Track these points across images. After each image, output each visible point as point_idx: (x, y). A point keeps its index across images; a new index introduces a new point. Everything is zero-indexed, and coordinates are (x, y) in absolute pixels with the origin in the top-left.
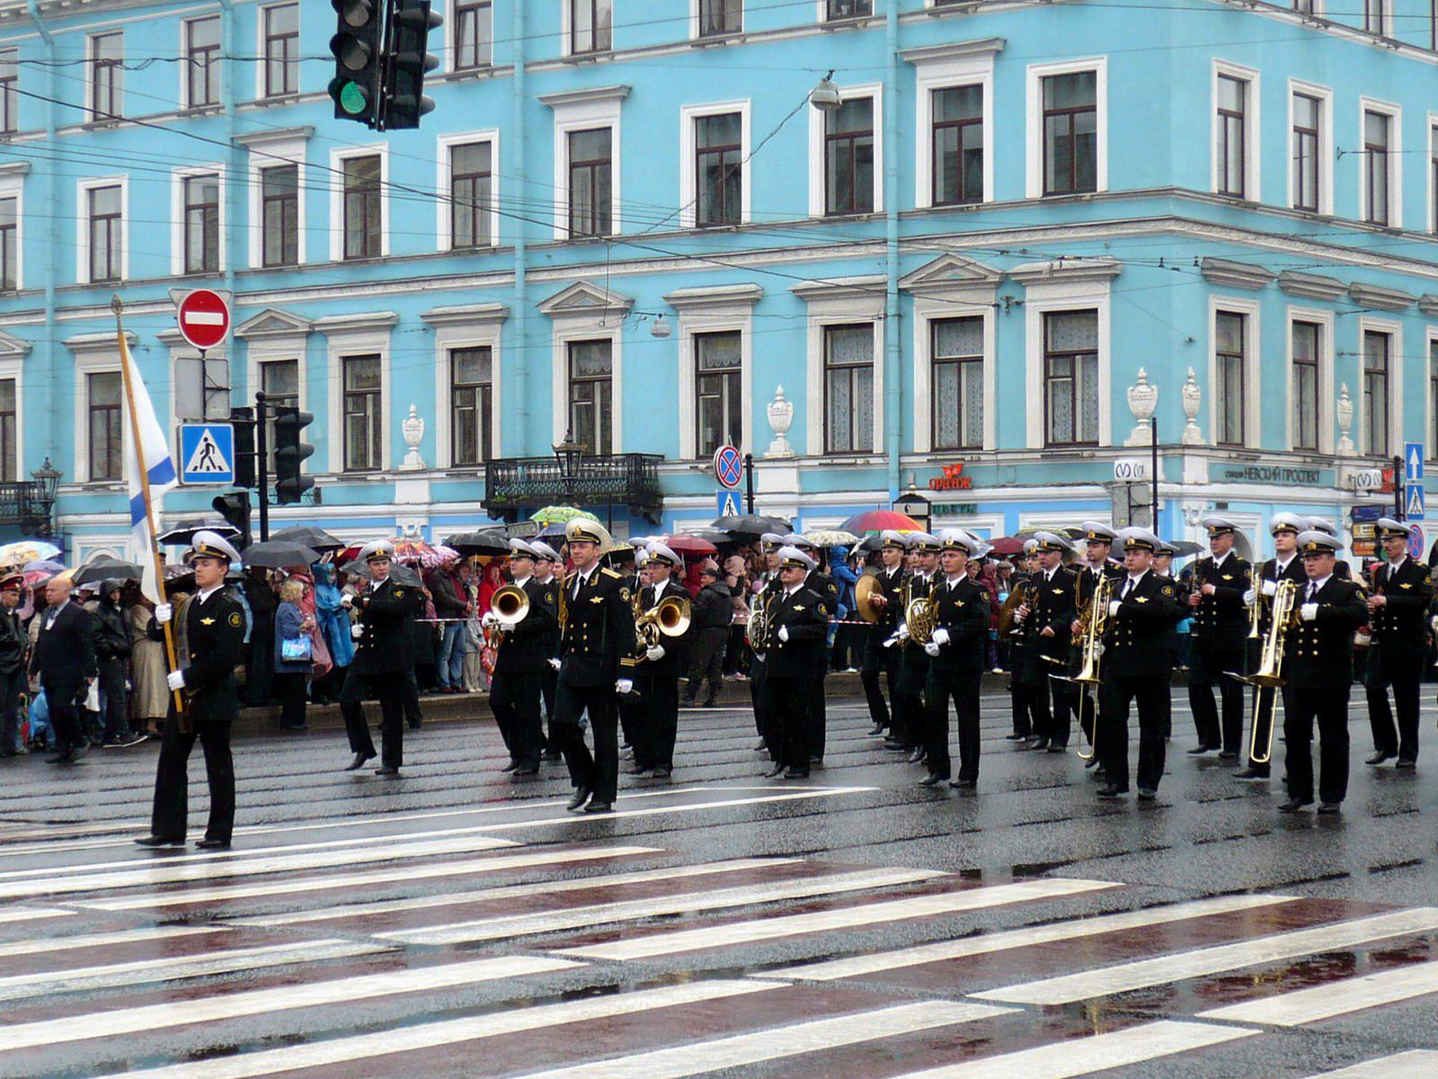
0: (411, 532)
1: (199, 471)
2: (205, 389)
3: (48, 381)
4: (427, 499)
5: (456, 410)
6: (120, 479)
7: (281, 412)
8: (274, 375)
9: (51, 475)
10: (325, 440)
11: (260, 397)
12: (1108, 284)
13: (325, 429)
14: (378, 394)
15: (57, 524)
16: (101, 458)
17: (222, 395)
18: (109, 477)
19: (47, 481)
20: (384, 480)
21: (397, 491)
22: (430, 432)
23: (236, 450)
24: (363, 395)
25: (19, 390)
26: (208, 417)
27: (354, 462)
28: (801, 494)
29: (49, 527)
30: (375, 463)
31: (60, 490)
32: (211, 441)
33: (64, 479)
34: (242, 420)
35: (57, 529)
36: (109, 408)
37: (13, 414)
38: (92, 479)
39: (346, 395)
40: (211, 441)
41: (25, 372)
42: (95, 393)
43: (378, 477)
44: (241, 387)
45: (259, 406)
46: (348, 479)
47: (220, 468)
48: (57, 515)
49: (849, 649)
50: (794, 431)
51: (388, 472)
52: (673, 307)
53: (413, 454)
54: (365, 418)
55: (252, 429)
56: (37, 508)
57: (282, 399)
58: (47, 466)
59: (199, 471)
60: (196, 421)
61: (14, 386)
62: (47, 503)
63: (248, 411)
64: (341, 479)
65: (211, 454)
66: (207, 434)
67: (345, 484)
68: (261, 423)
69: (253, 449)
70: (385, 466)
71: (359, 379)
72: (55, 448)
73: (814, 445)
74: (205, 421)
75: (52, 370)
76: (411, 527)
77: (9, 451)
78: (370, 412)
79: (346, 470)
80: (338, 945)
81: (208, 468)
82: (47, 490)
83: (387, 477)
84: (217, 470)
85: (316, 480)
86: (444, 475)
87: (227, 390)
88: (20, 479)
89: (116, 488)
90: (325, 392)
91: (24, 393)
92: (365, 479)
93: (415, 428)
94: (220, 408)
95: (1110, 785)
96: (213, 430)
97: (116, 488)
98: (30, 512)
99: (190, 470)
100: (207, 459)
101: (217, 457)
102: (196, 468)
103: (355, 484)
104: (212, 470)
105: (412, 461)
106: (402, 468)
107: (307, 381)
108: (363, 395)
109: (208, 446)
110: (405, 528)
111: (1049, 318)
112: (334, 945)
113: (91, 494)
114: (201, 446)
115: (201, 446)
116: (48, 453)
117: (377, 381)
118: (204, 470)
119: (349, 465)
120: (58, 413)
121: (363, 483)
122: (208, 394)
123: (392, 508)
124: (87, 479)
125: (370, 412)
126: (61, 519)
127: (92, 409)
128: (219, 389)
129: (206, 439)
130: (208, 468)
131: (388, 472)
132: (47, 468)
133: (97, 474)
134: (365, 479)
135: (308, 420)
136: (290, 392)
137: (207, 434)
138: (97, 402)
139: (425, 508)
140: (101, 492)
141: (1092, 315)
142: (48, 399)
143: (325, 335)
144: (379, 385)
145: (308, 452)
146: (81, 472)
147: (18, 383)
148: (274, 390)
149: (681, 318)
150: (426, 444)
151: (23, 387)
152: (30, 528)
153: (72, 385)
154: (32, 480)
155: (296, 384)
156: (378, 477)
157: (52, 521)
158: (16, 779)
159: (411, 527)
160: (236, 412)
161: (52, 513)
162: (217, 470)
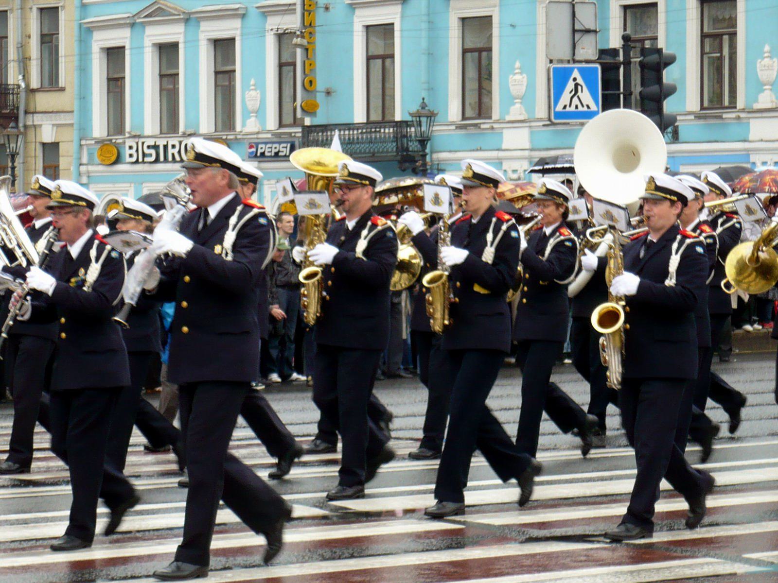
0: (515, 176)
1: (568, 109)
2: (574, 31)
3: (424, 26)
4: (527, 146)
5: (705, 57)
6: (490, 118)
7: (644, 52)
8: (635, 16)
9: (426, 114)
10: (683, 78)
11: (626, 38)
12: (183, 24)
13: (683, 70)
14: (733, 35)
15: (432, 161)
16: (472, 98)
17: (589, 38)
18: (480, 115)
19: (424, 120)
20: (738, 118)
21: (751, 124)
22: (531, 86)
23: (603, 89)
24: (719, 36)
25: (397, 34)
26: (577, 58)
27: (710, 101)
28: (531, 150)
29: (425, 164)
30: (730, 103)
31: (435, 128)
32: (580, 81)
33: (438, 118)
34: (608, 60)
35: (432, 166)
36: (480, 51)
37: (392, 56)
38: (464, 118)
39: (704, 36)
40: (580, 81)
41: (402, 17)
42: (467, 35)
43: (733, 115)
44: (606, 29)
45: (625, 47)
46: (705, 117)
47: (588, 107)
48: (432, 152)
49: (708, 282)
50: (527, 98)
51: (743, 110)
52: (264, 13)
53: (518, 106)
54: (721, 59)
55: (618, 68)
56: (414, 146)
57: (642, 41)
58: (424, 106)
59: (568, 109)
60: (569, 62)
61: (393, 29)
62: (423, 141)
63: (614, 52)
64: (698, 117)
65: (579, 93)
66: (576, 74)
67: (702, 122)
68: (627, 63)
69: (619, 89)
70: (740, 103)
71: (715, 21)
72: (431, 89)
73: (541, 112)
74: (575, 61)
75: (429, 15)
76: (764, 163)
77: (388, 92)
78: (726, 51)
79: (702, 108)
80: (711, 563)
81: (577, 107)
82: (424, 128)
83: (742, 115)
84: (585, 109)
85: (679, 118)
86: (692, 117)
87: (595, 32)
88: (398, 118)
89: (487, 126)
90: (683, 34)
91: (402, 37)
92: (720, 117)
93: (769, 68)
94: (588, 49)
95: (307, 377)
96: (581, 70)
97: (487, 126)
98: (407, 150)
99: (559, 108)
100: (575, 99)
101: (586, 96)
102: (565, 107)
103: (712, 121)
104: (580, 108)
105: (516, 112)
106: (756, 106)
107: (667, 23)
108: (719, 36)
109: (577, 85)
110: (510, 172)
111: (628, 11)
112: (707, 564)
113: (463, 132)
114: (571, 85)
115: (571, 85)
116: (424, 94)
117: (732, 22)
118: (573, 108)
119: (706, 104)
120: (433, 56)
121: (478, 131)
122: (577, 36)
123: (501, 154)
124: (460, 117)
125: (726, 51)
126: (435, 156)
127: (465, 51)
128: (588, 31)
129: (575, 79)
130: (577, 107)
131: (743, 110)
132: (423, 108)
133: (469, 113)
134: (720, 117)
135: (670, 61)
136: (650, 34)
137: (576, 74)
138: (469, 45)
139: (526, 153)
140: (472, 130)
141: (652, 9)
142: (424, 44)
143: (199, 20)
144: (734, 26)
145: (672, 90)
146: (453, 111)
147: (397, 27)
148: (636, 32)
149: (202, 28)
150: (260, 112)
151: (401, 31)
152: (407, 165)
153: (447, 29)
154: (409, 118)
155: (656, 26)
156: (733, 115)
157: (428, 158)
158: (400, 400)
159: (514, 171)
160: (603, 52)
161: (428, 150)
162: (585, 109)
